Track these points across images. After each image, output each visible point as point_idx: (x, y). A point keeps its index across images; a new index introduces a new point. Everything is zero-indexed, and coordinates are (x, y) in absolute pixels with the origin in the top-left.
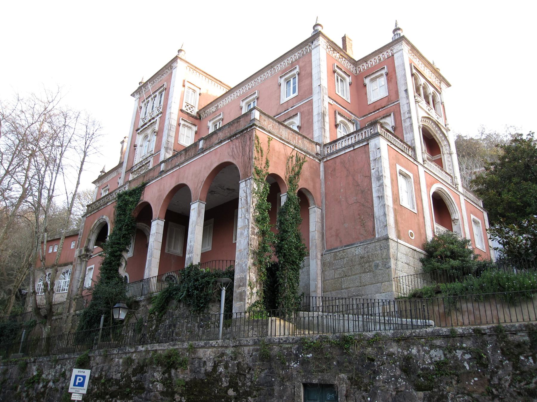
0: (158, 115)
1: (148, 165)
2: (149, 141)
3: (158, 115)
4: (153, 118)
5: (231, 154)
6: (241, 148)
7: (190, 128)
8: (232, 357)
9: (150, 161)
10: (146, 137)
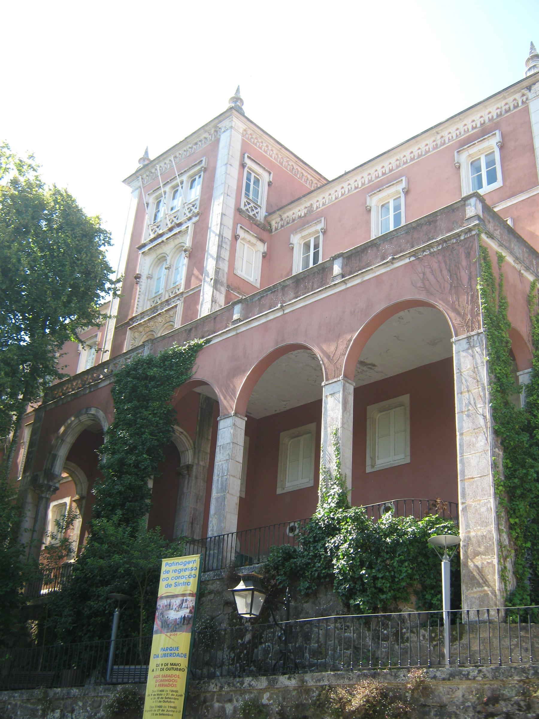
0: (190, 219)
1: (171, 313)
2: (168, 268)
3: (190, 219)
4: (179, 225)
5: (420, 284)
6: (445, 272)
7: (253, 245)
8: (519, 705)
9: (176, 306)
10: (162, 259)
